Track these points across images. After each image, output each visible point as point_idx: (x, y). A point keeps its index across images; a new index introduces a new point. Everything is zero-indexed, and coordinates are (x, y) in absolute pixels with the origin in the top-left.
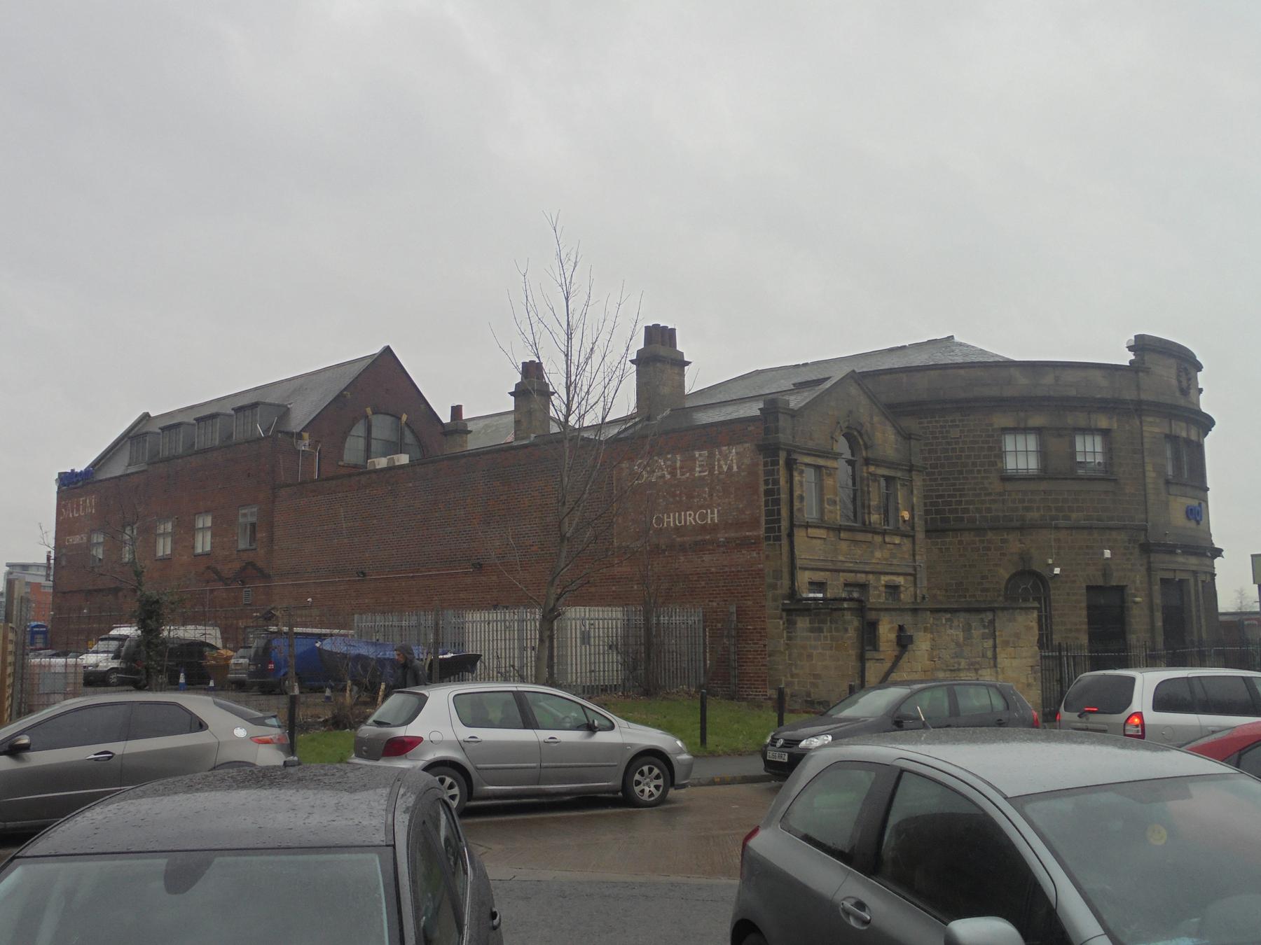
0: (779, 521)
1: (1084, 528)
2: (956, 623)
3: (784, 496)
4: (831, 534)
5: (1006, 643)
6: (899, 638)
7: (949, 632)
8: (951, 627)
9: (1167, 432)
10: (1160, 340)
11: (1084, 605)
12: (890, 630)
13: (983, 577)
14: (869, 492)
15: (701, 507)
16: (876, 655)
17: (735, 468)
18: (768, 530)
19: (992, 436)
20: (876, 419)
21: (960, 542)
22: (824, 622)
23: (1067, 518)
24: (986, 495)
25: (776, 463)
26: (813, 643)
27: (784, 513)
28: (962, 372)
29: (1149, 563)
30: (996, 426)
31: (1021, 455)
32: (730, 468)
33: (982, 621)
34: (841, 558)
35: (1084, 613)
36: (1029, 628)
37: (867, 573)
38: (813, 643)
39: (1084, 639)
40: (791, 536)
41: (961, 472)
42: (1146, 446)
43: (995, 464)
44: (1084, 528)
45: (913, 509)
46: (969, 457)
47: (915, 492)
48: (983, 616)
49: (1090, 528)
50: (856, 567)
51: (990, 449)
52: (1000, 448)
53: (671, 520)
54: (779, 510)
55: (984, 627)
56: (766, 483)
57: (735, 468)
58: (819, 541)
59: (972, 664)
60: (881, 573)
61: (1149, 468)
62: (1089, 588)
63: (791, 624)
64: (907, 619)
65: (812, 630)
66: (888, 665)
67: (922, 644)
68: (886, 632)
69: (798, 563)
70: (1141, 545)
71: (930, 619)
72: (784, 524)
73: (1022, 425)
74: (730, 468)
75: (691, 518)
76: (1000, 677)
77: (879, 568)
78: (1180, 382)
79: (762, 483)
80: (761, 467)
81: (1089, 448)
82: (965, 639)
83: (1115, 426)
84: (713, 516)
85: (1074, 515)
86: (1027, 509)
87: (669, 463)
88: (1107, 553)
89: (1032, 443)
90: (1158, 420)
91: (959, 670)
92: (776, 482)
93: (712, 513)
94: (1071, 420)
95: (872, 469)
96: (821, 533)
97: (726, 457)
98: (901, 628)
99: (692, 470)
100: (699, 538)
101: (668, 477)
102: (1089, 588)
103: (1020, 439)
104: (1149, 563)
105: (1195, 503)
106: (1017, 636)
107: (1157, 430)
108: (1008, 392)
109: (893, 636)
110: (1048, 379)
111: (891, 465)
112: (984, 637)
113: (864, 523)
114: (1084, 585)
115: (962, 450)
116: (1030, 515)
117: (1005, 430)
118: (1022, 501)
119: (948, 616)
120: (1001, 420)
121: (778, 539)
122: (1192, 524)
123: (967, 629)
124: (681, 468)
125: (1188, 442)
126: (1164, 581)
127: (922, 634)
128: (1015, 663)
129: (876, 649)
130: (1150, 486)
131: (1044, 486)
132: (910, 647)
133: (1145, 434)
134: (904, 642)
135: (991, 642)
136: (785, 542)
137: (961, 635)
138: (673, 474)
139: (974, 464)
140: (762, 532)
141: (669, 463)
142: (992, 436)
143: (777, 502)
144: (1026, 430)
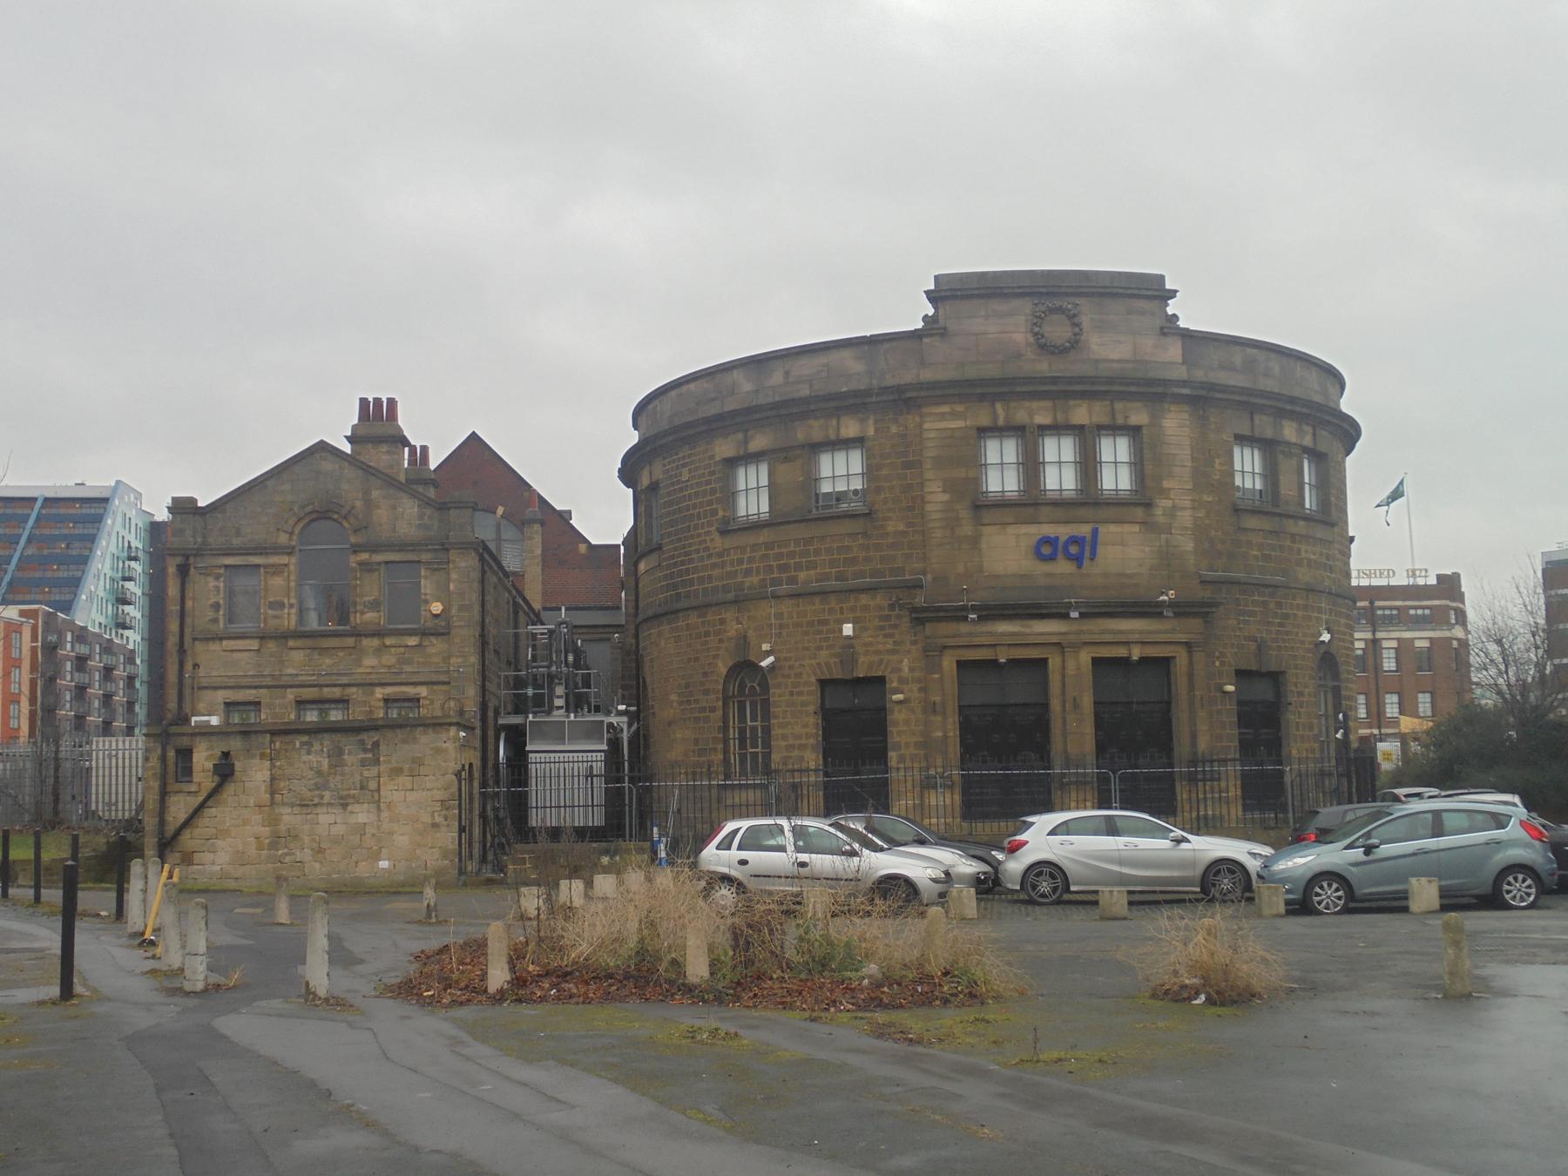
1: (814, 594)
2: (316, 747)
7: (305, 758)
8: (309, 753)
10: (983, 276)
13: (705, 674)
16: (185, 787)
23: (792, 580)
28: (692, 386)
33: (362, 742)
34: (290, 671)
37: (344, 686)
39: (813, 759)
44: (814, 594)
48: (364, 736)
49: (823, 593)
55: (365, 751)
59: (341, 798)
60: (374, 685)
62: (823, 683)
67: (255, 774)
68: (203, 759)
76: (385, 814)
77: (374, 678)
81: (841, 470)
82: (331, 766)
86: (748, 572)
88: (848, 629)
90: (960, 408)
94: (803, 432)
95: (364, 556)
102: (823, 683)
103: (840, 457)
106: (418, 762)
107: (959, 424)
108: (731, 405)
110: (777, 378)
114: (813, 679)
118: (740, 562)
119: (305, 738)
120: (724, 448)
123: (337, 754)
127: (256, 761)
128: (411, 796)
134: (225, 771)
137: (325, 763)
144: (845, 444)
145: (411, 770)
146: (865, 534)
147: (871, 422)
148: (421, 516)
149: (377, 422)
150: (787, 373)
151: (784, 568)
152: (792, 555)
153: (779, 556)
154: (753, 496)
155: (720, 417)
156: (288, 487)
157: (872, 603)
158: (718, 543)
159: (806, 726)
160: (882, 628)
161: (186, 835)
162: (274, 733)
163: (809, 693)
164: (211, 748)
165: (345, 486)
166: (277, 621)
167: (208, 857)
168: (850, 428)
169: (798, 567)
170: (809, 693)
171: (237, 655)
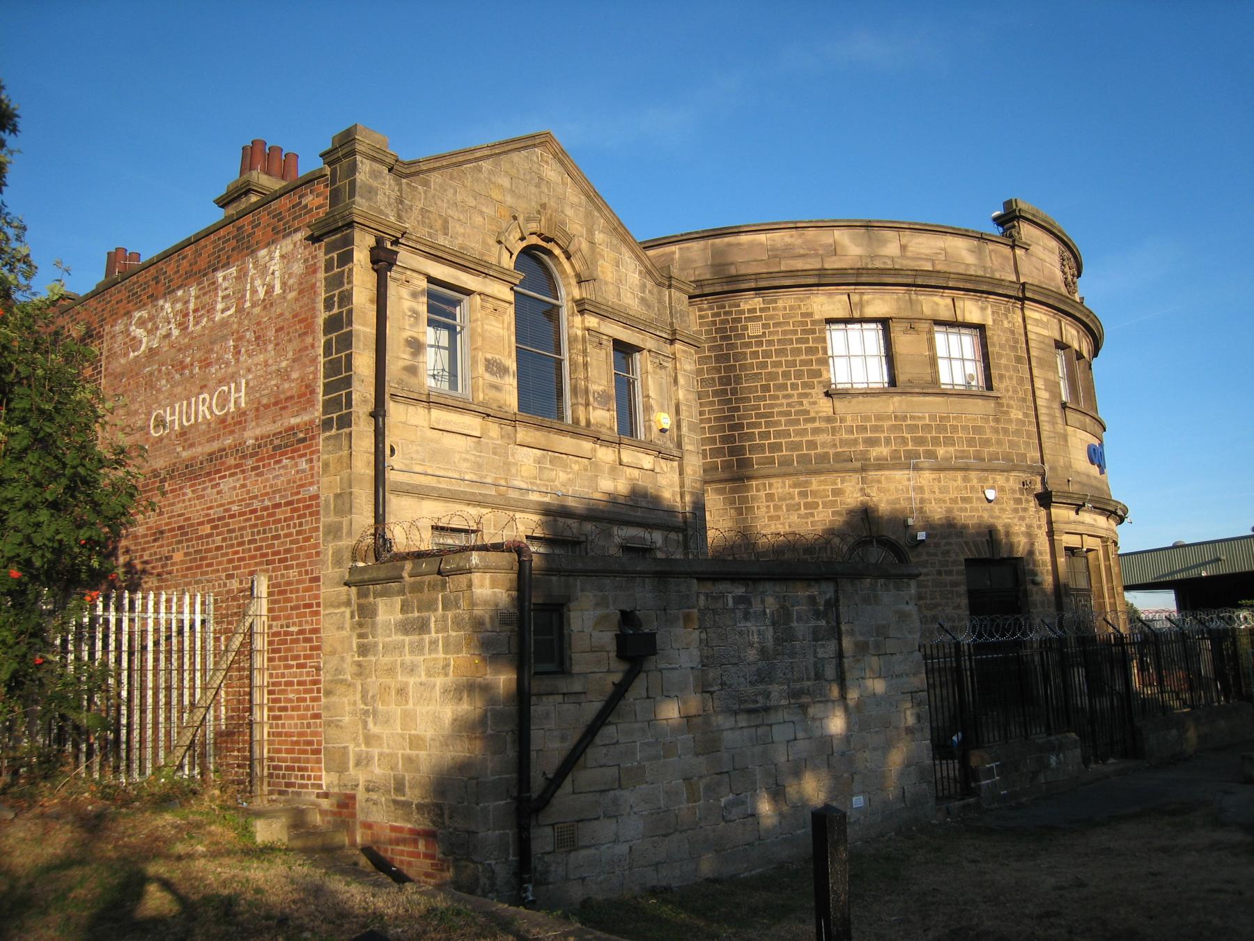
0: (348, 382)
3: (364, 328)
4: (494, 429)
5: (862, 648)
6: (622, 642)
8: (746, 616)
9: (1058, 338)
11: (963, 589)
12: (600, 622)
14: (586, 365)
15: (221, 382)
16: (563, 685)
17: (278, 290)
18: (329, 406)
19: (813, 331)
20: (599, 237)
21: (770, 497)
22: (431, 606)
23: (931, 455)
24: (806, 421)
25: (347, 258)
26: (408, 658)
27: (363, 363)
29: (1050, 523)
30: (816, 317)
31: (855, 358)
32: (270, 291)
35: (964, 602)
36: (903, 616)
38: (408, 658)
40: (378, 413)
41: (766, 388)
42: (1034, 353)
43: (818, 374)
45: (678, 412)
46: (777, 364)
47: (681, 381)
51: (810, 351)
52: (825, 350)
53: (175, 417)
54: (349, 358)
55: (817, 614)
56: (328, 304)
57: (278, 290)
58: (461, 442)
61: (1039, 384)
63: (365, 613)
64: (642, 597)
65: (405, 628)
66: (593, 707)
67: (682, 648)
69: (391, 476)
70: (1038, 496)
71: (700, 594)
72: (363, 391)
73: (857, 315)
74: (270, 291)
75: (205, 408)
78: (1064, 273)
79: (321, 306)
80: (321, 275)
82: (778, 641)
83: (990, 322)
84: (239, 397)
85: (941, 451)
86: (872, 442)
87: (179, 306)
89: (872, 336)
90: (1045, 318)
91: (767, 709)
92: (346, 298)
93: (238, 390)
95: (592, 321)
96: (472, 423)
97: (264, 270)
98: (627, 618)
99: (211, 310)
100: (216, 445)
101: (176, 332)
104: (1050, 523)
105: (1096, 442)
106: (882, 631)
107: (1045, 332)
109: (607, 638)
111: (628, 321)
112: (816, 636)
113: (576, 421)
114: (962, 558)
115: (767, 354)
116: (874, 452)
117: (830, 321)
119: (740, 590)
120: (826, 304)
121: (345, 421)
122: (1095, 470)
124: (196, 311)
125: (1080, 356)
126: (1071, 551)
129: (563, 669)
130: (1042, 411)
131: (895, 404)
132: (650, 664)
133: (1030, 336)
134: (635, 647)
135: (832, 647)
136: (363, 431)
138: (183, 326)
139: (786, 375)
140: (317, 413)
141: (179, 306)
142: (813, 331)
143: (346, 341)
146: (997, 421)
147: (989, 311)
148: (643, 286)
149: (5, 185)
150: (903, 248)
151: (920, 441)
152: (927, 427)
153: (912, 428)
154: (857, 363)
155: (821, 272)
156: (505, 182)
157: (952, 484)
158: (825, 406)
159: (958, 607)
160: (1016, 510)
161: (564, 794)
162: (702, 578)
163: (958, 573)
164: (602, 603)
165: (569, 212)
166: (493, 394)
167: (606, 829)
168: (972, 311)
169: (936, 442)
170: (958, 573)
171: (448, 440)
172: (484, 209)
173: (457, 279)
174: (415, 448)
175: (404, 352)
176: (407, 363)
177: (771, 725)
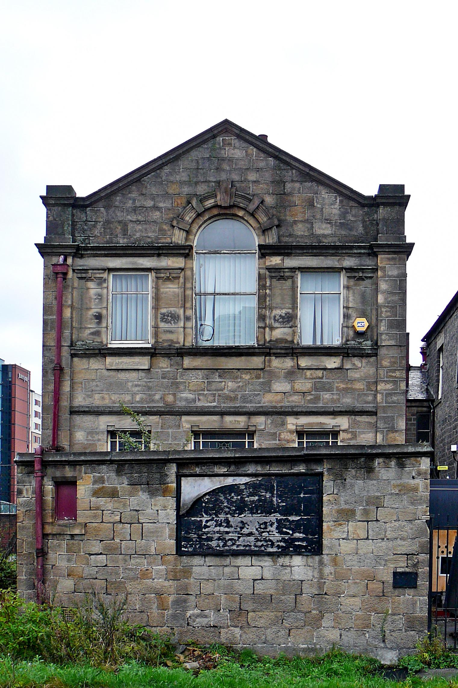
5: (346, 515)
50: (226, 405)
145: (366, 512)
171: (122, 376)
172: (161, 205)
173: (135, 263)
174: (94, 383)
175: (90, 324)
176: (92, 330)
177: (238, 567)
